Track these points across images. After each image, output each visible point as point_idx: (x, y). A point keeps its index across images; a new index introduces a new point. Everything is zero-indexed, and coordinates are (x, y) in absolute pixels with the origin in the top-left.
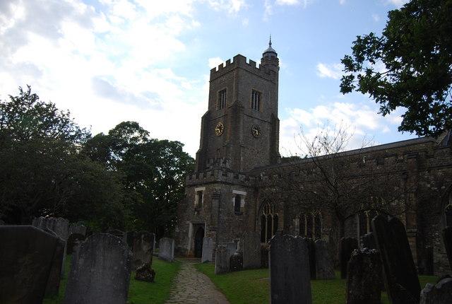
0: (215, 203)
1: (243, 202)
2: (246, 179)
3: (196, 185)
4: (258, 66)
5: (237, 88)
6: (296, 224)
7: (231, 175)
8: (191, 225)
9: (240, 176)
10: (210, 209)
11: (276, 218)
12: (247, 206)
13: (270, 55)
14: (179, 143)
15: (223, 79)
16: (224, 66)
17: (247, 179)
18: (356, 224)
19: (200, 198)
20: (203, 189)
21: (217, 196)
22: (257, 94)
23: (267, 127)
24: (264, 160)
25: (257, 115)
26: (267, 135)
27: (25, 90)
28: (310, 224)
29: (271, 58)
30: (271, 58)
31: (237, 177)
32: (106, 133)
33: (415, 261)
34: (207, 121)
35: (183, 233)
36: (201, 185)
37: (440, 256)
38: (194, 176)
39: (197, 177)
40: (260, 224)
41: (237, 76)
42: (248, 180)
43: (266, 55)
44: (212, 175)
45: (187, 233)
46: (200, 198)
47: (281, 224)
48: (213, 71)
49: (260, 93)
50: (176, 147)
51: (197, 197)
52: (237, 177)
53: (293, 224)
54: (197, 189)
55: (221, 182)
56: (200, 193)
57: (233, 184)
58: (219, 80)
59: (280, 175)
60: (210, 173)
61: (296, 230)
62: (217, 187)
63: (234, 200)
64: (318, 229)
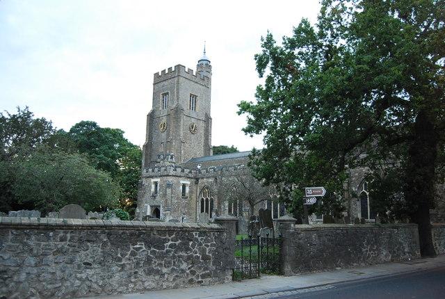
0: (169, 191)
1: (187, 190)
2: (189, 172)
3: (152, 177)
4: (194, 74)
5: (178, 93)
7: (179, 170)
8: (149, 208)
9: (185, 170)
10: (165, 195)
11: (212, 201)
12: (191, 192)
13: (205, 62)
14: (120, 130)
15: (166, 83)
16: (167, 72)
17: (190, 172)
19: (156, 186)
20: (158, 180)
21: (169, 186)
22: (193, 97)
23: (202, 124)
24: (199, 152)
25: (194, 115)
26: (201, 131)
27: (22, 109)
28: (235, 207)
29: (205, 66)
30: (205, 66)
31: (183, 171)
32: (67, 130)
33: (270, 62)
34: (152, 118)
36: (156, 177)
38: (150, 170)
39: (153, 171)
40: (200, 204)
41: (178, 81)
42: (190, 172)
43: (200, 62)
44: (165, 170)
46: (156, 186)
47: (215, 204)
48: (156, 75)
49: (196, 96)
50: (117, 135)
51: (153, 186)
52: (183, 171)
54: (153, 180)
55: (173, 176)
56: (156, 183)
57: (180, 177)
58: (162, 84)
59: (214, 170)
60: (164, 168)
62: (170, 179)
64: (241, 210)
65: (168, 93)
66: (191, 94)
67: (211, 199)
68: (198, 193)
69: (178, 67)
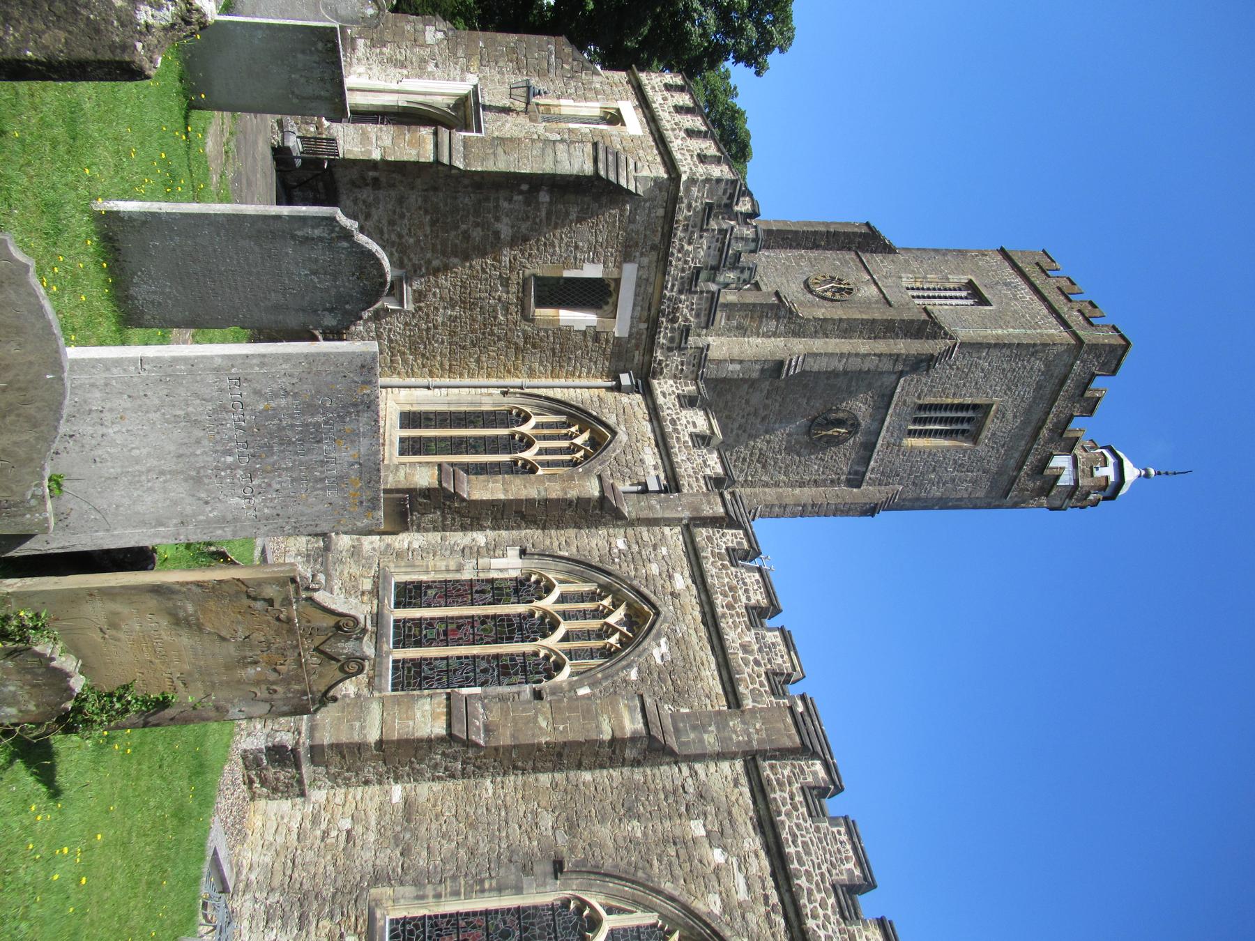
6: (496, 563)
18: (518, 890)
35: (423, 61)
37: (964, 279)
45: (422, 73)
49: (974, 437)
53: (493, 550)
54: (628, 109)
56: (615, 118)
58: (1018, 280)
61: (470, 564)
63: (592, 271)
65: (983, 301)
66: (990, 406)
67: (528, 468)
68: (558, 394)
69: (873, 515)
